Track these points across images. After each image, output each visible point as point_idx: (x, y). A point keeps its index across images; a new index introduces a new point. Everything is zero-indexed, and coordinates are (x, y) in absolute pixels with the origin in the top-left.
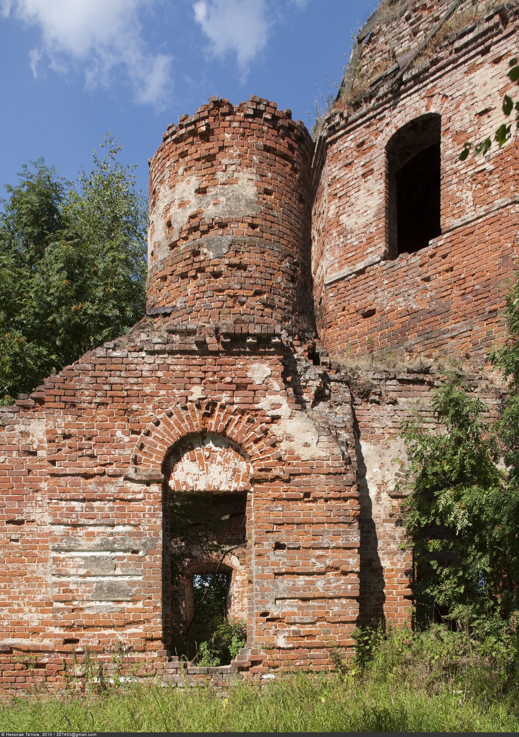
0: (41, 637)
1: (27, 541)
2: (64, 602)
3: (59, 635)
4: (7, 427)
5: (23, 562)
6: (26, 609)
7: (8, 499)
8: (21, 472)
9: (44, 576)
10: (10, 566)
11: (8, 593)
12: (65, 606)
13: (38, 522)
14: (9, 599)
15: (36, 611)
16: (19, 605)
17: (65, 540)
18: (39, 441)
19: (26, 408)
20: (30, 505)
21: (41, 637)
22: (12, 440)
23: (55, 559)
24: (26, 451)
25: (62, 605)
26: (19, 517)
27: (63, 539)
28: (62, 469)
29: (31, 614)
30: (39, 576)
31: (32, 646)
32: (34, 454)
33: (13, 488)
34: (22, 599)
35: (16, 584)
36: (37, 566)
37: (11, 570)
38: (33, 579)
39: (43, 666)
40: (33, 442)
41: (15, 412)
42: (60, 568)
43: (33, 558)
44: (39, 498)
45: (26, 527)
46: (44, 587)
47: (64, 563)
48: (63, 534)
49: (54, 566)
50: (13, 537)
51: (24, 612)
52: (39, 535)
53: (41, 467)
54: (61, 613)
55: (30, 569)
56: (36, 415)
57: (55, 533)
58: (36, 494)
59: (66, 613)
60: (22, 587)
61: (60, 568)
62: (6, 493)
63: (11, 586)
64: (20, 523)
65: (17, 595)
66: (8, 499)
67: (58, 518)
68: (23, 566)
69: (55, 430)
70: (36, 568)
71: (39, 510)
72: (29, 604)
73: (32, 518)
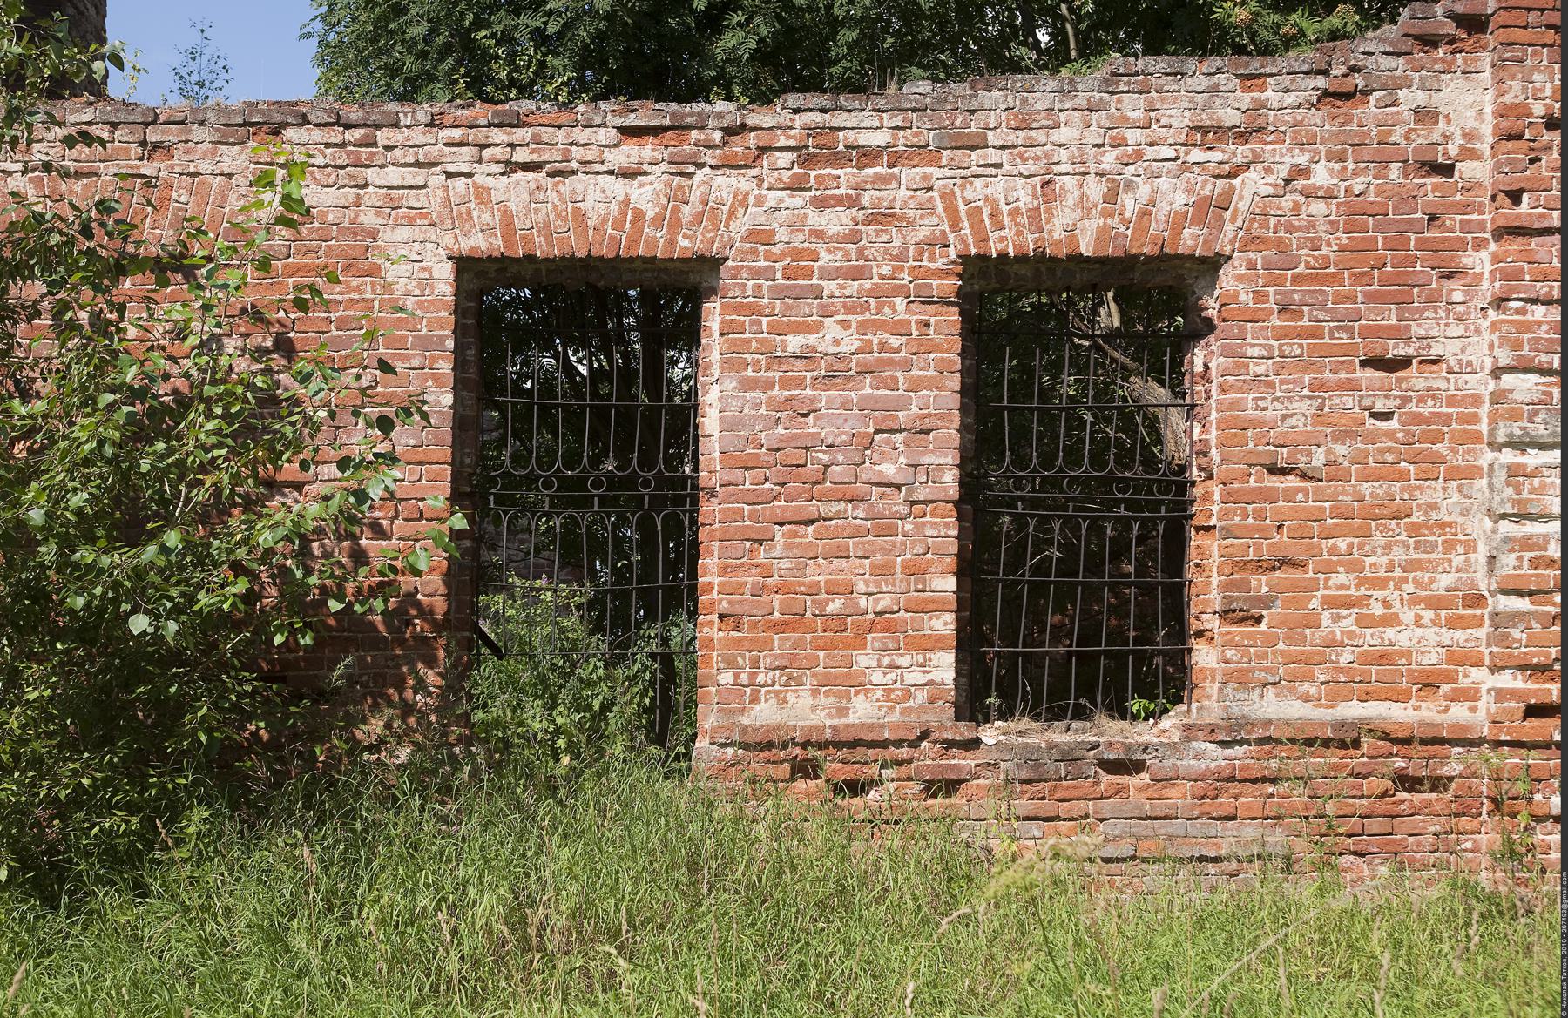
0: (1446, 697)
1: (1418, 419)
2: (1530, 594)
3: (1513, 694)
4: (1377, 94)
5: (1402, 477)
6: (1408, 616)
7: (1370, 298)
8: (1410, 221)
9: (1461, 520)
10: (1366, 488)
11: (1355, 567)
12: (1533, 608)
13: (1453, 362)
14: (1358, 586)
15: (1436, 623)
16: (1386, 603)
17: (1542, 416)
18: (1464, 135)
19: (1429, 42)
20: (1432, 315)
21: (1446, 697)
22: (1390, 133)
23: (1514, 471)
24: (1424, 164)
25: (1523, 604)
26: (1396, 350)
27: (1536, 413)
28: (1541, 216)
29: (1419, 631)
30: (1447, 519)
31: (1421, 724)
32: (1447, 170)
33: (1385, 265)
34: (1398, 588)
35: (1382, 541)
36: (1444, 489)
37: (1368, 501)
38: (1430, 528)
39: (1438, 784)
40: (1447, 137)
41: (1399, 55)
42: (1525, 495)
43: (1430, 466)
44: (1458, 296)
45: (1416, 379)
46: (1461, 549)
47: (1536, 482)
48: (1536, 397)
49: (1510, 490)
50: (1380, 407)
51: (1400, 623)
52: (1452, 402)
53: (1467, 207)
54: (1522, 626)
55: (1423, 499)
56: (1460, 62)
57: (1515, 396)
58: (1447, 285)
59: (1537, 628)
60: (1397, 550)
61: (1525, 495)
62: (1365, 280)
63: (1367, 548)
64: (1398, 364)
65: (1382, 573)
66: (1370, 298)
67: (1525, 351)
68: (1403, 490)
69: (1526, 107)
70: (1440, 494)
71: (1456, 330)
72: (1414, 600)
73: (1436, 351)
